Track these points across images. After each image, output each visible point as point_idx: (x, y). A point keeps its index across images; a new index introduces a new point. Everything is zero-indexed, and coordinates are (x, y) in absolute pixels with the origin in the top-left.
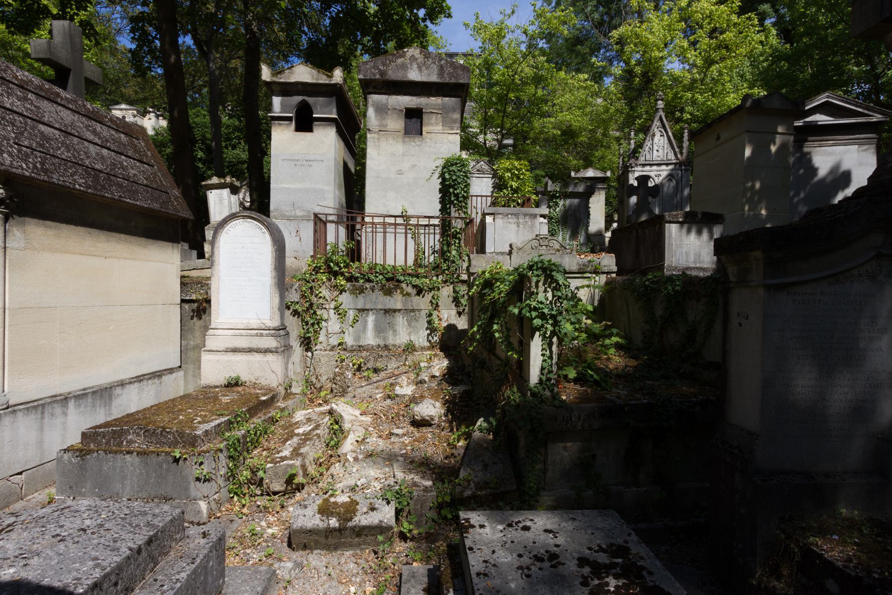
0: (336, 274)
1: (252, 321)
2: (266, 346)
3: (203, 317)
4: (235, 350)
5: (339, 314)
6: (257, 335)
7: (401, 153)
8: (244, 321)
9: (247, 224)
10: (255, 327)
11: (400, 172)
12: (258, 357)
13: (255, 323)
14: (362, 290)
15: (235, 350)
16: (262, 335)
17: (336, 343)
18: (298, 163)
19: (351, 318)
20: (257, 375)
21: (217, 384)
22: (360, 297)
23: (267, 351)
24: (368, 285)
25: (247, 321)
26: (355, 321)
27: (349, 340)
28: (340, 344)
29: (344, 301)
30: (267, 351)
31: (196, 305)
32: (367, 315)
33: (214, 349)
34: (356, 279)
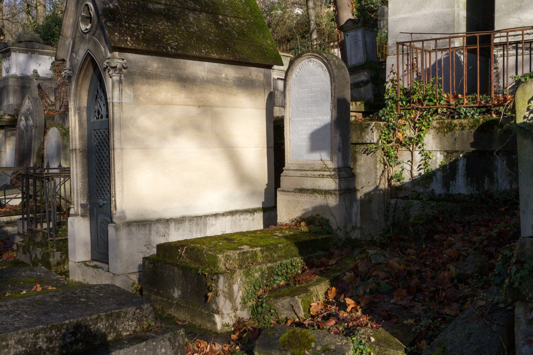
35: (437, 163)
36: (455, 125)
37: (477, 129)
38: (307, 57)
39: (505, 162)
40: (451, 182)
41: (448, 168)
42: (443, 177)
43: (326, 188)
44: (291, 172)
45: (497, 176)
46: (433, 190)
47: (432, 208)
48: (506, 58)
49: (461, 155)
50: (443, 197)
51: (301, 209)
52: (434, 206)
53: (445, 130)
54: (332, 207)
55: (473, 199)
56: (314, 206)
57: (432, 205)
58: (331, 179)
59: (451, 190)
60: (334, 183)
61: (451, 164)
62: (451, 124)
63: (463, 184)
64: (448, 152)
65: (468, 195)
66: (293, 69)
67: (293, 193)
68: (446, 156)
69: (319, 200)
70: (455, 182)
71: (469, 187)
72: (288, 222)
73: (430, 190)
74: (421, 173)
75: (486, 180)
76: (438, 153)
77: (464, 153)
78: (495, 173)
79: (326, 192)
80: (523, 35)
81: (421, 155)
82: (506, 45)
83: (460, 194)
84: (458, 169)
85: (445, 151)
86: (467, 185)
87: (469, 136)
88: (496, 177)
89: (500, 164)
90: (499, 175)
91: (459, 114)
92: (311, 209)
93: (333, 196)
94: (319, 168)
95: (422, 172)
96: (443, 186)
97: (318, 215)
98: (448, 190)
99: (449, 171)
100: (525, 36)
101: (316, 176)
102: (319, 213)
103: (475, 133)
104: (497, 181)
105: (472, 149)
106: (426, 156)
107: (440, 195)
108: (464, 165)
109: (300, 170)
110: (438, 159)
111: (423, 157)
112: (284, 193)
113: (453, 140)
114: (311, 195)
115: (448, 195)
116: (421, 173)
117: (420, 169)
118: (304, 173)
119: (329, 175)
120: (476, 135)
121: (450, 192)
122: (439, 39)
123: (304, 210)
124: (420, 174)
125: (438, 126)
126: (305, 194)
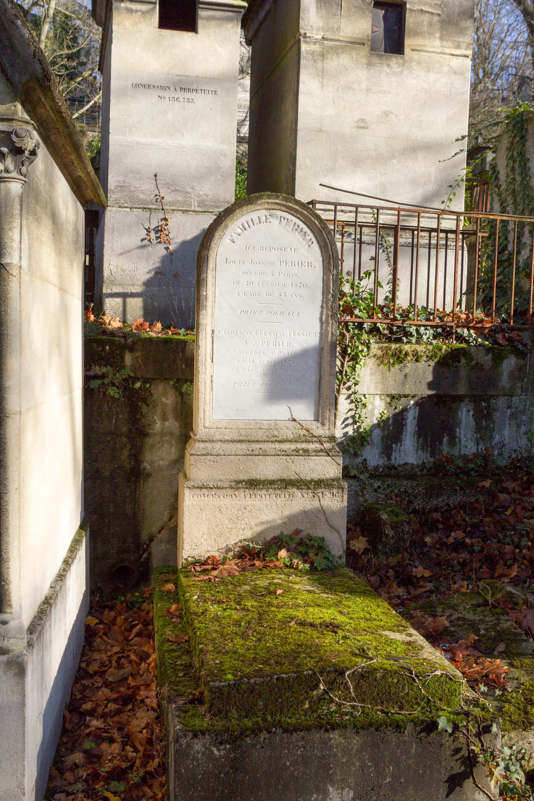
16: (306, 452)
35: (373, 415)
36: (406, 354)
37: (439, 362)
38: (267, 206)
39: (471, 413)
40: (394, 446)
41: (391, 422)
42: (383, 438)
43: (316, 476)
44: (218, 445)
45: (460, 433)
46: (365, 460)
47: (376, 491)
48: (415, 249)
49: (412, 402)
50: (381, 470)
51: (253, 522)
52: (379, 487)
53: (391, 361)
54: (333, 513)
55: (425, 471)
56: (287, 513)
57: (376, 485)
58: (328, 458)
59: (393, 458)
60: (335, 466)
61: (395, 416)
62: (401, 352)
63: (411, 448)
64: (393, 397)
65: (418, 466)
66: (226, 226)
67: (229, 492)
68: (390, 404)
69: (300, 502)
70: (401, 446)
71: (420, 452)
72: (216, 554)
73: (360, 460)
74: (347, 433)
75: (445, 439)
76: (378, 398)
77: (416, 399)
78: (457, 430)
79: (318, 485)
80: (335, 211)
81: (349, 401)
82: (417, 230)
83: (406, 464)
84: (406, 425)
85: (388, 396)
86: (417, 450)
87: (425, 371)
88: (458, 434)
89: (465, 416)
90: (462, 432)
91: (408, 334)
92: (279, 522)
93: (335, 491)
94: (290, 436)
95: (350, 430)
96: (382, 453)
97: (297, 532)
98: (389, 459)
99: (392, 428)
100: (338, 213)
101: (289, 452)
102: (300, 527)
103: (434, 369)
104: (460, 441)
105: (430, 392)
106: (358, 403)
107: (376, 468)
108: (414, 418)
109: (241, 441)
110: (376, 409)
111: (353, 406)
112: (205, 491)
113: (401, 376)
114: (279, 492)
115: (388, 467)
116: (347, 433)
117: (346, 426)
118: (254, 446)
119: (321, 450)
120: (436, 371)
121: (393, 462)
122: (383, 208)
123: (262, 523)
124: (346, 434)
125: (379, 353)
126: (264, 492)
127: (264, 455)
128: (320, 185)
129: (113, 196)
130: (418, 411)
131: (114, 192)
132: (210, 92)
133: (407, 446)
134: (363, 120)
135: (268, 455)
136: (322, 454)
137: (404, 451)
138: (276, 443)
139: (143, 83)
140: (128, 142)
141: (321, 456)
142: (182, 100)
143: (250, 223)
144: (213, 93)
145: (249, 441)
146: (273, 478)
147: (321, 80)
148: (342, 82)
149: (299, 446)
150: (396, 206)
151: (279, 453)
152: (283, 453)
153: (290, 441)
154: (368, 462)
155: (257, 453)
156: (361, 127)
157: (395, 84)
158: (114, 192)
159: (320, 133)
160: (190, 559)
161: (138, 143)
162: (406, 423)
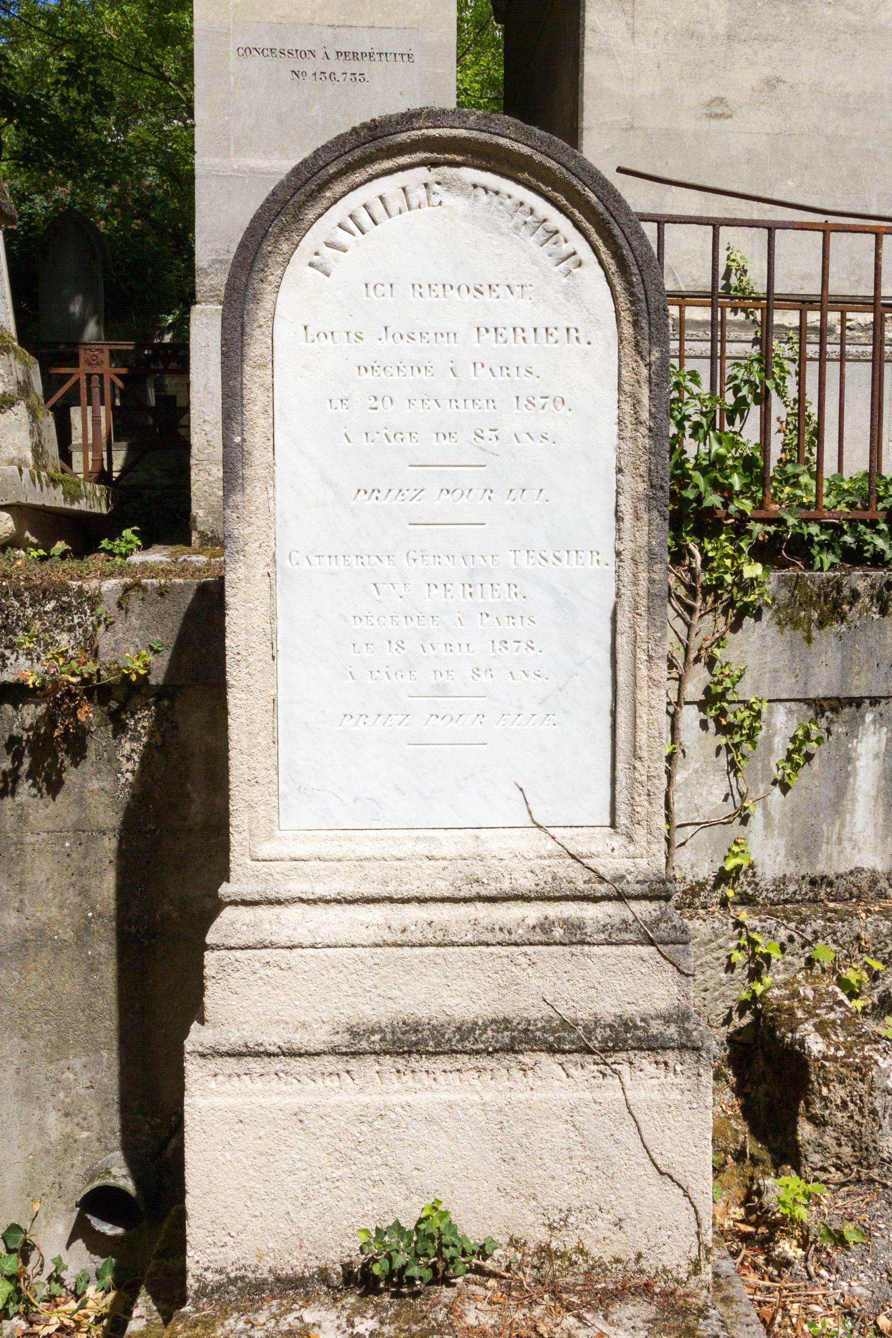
0: (706, 524)
1: (495, 844)
2: (608, 1008)
3: (71, 776)
4: (409, 1043)
5: (726, 730)
6: (544, 935)
7: (721, 27)
8: (449, 845)
9: (453, 201)
10: (526, 884)
11: (717, 109)
12: (556, 1086)
13: (519, 858)
14: (833, 606)
15: (409, 1043)
16: (576, 936)
17: (706, 871)
18: (308, 66)
19: (781, 745)
20: (561, 1195)
21: (295, 1264)
22: (827, 640)
23: (616, 1041)
24: (859, 580)
25: (464, 843)
26: (799, 754)
27: (768, 855)
28: (723, 877)
29: (752, 661)
30: (616, 1041)
31: (30, 713)
32: (854, 725)
33: (273, 1039)
34: (801, 548)
62: (839, 587)
63: (870, 830)
108: (876, 756)
127: (439, 945)
128: (620, 170)
129: (206, 282)
130: (884, 738)
131: (207, 274)
132: (399, 57)
133: (859, 827)
134: (721, 100)
135: (453, 944)
136: (627, 936)
137: (850, 839)
138: (479, 905)
139: (260, 46)
140: (233, 170)
141: (625, 943)
142: (340, 77)
143: (378, 209)
144: (405, 57)
145: (391, 900)
146: (470, 1017)
147: (630, 21)
148: (675, 22)
149: (554, 911)
150: (820, 218)
151: (487, 937)
152: (500, 937)
153: (525, 898)
154: (759, 870)
155: (417, 937)
156: (717, 116)
157: (788, 19)
158: (207, 274)
159: (631, 133)
160: (209, 1276)
161: (252, 171)
162: (855, 768)
